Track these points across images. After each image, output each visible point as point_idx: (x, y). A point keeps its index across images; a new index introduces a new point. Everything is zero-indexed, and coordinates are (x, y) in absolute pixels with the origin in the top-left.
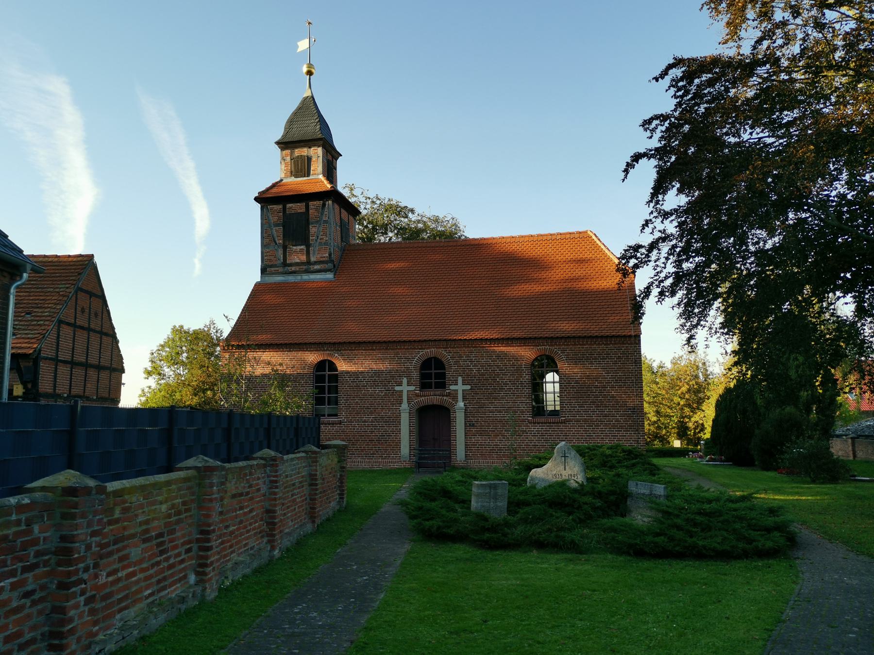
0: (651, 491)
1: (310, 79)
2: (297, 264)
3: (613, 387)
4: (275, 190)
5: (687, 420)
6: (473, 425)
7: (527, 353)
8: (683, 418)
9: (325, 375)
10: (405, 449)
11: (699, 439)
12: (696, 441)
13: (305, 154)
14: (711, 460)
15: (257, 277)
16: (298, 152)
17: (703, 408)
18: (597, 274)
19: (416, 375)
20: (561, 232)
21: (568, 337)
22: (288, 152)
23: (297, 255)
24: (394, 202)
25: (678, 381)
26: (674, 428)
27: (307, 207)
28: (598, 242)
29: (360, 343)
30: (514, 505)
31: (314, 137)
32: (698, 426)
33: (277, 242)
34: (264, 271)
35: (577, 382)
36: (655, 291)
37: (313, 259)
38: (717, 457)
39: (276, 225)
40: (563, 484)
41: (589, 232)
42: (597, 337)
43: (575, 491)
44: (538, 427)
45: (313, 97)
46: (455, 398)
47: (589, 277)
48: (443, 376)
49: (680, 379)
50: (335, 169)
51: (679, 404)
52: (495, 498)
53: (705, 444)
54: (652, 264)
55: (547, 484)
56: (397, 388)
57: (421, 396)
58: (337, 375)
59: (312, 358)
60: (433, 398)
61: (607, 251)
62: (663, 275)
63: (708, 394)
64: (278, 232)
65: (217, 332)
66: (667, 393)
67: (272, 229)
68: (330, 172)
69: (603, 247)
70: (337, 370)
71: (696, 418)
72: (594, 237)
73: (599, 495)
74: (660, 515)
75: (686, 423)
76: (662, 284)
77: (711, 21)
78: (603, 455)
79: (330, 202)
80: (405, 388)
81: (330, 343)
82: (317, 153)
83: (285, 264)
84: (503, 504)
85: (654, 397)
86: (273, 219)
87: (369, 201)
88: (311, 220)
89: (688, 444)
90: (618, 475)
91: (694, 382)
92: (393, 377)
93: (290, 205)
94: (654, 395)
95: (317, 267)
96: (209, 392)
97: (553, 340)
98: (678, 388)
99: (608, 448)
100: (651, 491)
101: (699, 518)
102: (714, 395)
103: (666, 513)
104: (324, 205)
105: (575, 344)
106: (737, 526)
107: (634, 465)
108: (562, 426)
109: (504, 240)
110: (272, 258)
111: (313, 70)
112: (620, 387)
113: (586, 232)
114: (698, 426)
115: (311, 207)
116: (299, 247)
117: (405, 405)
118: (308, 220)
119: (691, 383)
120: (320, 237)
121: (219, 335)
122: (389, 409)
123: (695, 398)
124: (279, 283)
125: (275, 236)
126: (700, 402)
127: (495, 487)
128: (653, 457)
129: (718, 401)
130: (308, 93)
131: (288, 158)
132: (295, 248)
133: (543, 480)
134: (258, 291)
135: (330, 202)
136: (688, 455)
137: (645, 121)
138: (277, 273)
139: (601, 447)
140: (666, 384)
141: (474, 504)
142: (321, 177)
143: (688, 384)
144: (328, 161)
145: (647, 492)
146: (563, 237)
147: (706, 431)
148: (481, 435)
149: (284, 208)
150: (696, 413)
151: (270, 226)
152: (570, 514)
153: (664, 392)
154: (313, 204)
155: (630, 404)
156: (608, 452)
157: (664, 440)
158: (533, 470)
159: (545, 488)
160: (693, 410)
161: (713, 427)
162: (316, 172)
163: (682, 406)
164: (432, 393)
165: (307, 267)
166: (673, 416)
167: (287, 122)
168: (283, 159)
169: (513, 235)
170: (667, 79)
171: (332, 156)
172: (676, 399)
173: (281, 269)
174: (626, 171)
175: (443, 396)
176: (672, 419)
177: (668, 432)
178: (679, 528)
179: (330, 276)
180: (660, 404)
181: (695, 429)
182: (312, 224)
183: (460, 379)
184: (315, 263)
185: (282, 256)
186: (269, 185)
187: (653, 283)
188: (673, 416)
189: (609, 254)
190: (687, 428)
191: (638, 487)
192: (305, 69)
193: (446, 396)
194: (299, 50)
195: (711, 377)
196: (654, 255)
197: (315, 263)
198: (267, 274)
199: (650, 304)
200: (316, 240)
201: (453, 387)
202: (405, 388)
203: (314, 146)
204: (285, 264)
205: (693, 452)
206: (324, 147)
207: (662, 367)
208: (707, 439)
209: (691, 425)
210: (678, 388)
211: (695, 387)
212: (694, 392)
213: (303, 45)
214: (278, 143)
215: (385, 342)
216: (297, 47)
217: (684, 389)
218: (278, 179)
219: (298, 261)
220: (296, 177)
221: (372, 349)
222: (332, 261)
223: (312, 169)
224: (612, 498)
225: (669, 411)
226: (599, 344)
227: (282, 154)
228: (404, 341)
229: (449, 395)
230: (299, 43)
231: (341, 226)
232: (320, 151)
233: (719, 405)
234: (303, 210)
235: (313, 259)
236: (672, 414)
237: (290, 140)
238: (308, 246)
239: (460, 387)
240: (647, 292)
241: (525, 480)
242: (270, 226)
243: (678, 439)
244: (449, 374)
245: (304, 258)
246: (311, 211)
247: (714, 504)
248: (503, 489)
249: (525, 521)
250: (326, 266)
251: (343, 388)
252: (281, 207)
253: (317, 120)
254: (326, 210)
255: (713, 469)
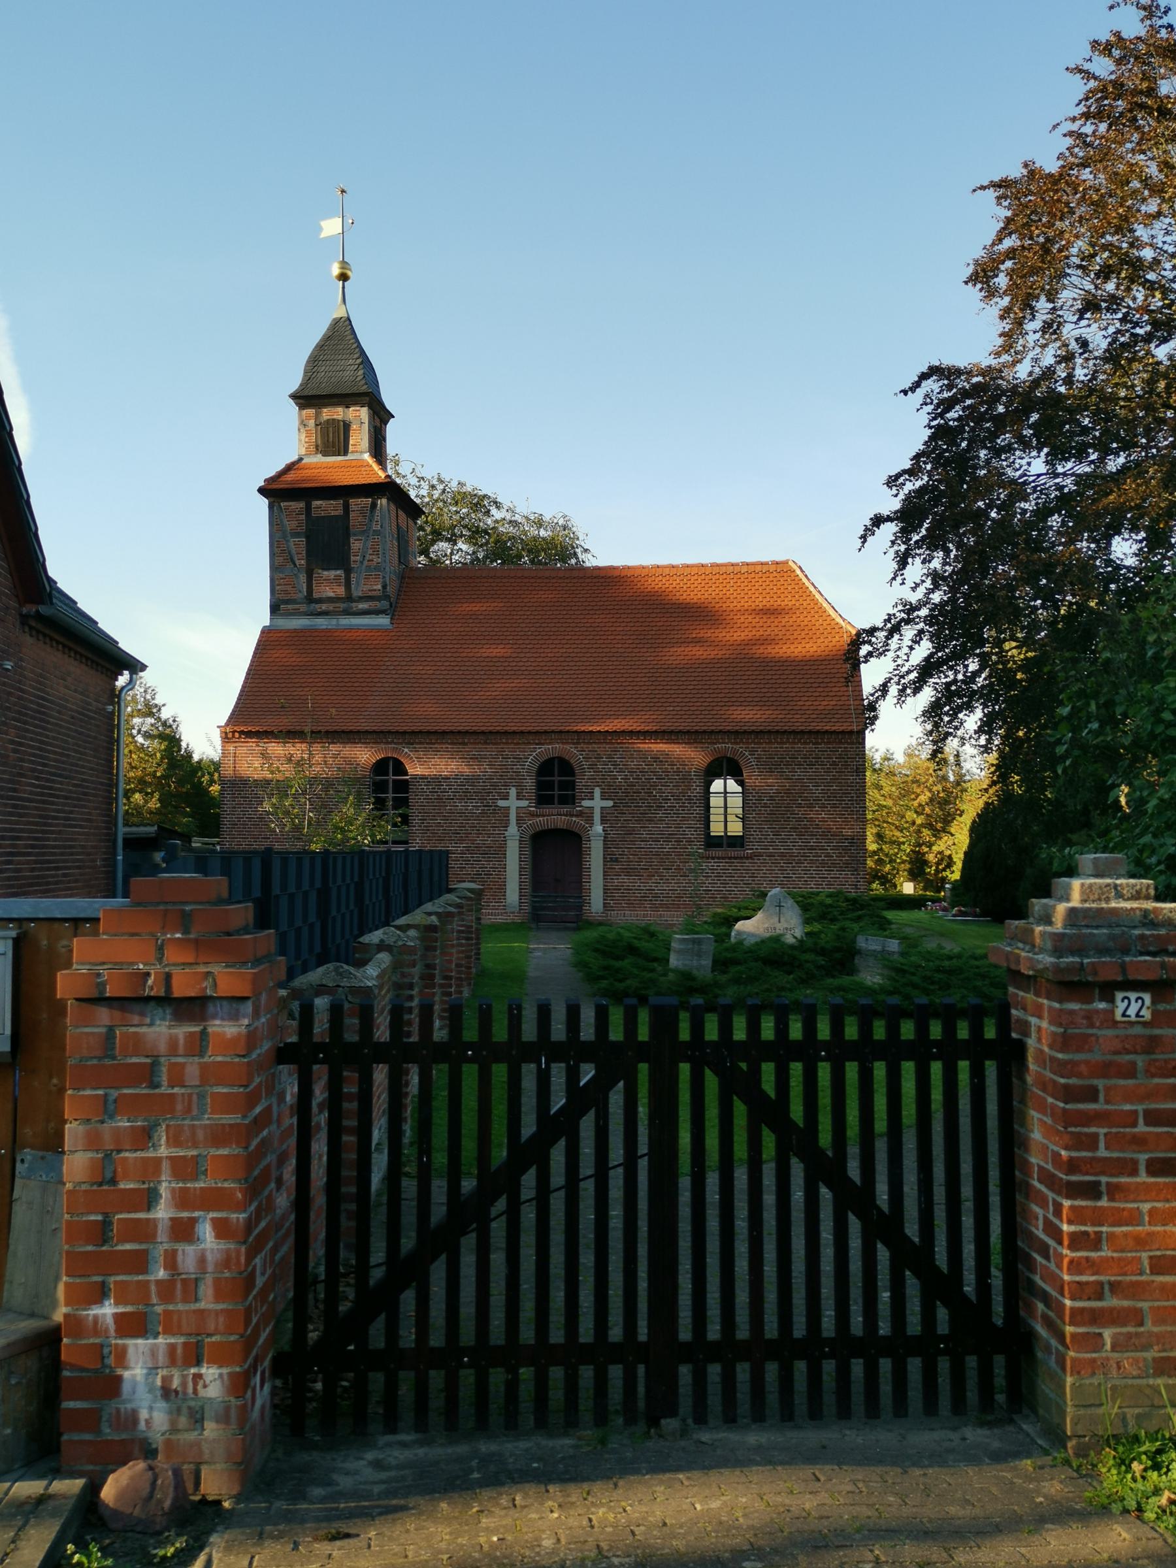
0: (884, 947)
1: (343, 288)
2: (330, 600)
3: (823, 806)
4: (290, 477)
5: (926, 849)
6: (616, 860)
7: (695, 756)
8: (920, 845)
9: (387, 781)
10: (512, 894)
11: (944, 880)
12: (938, 883)
13: (340, 417)
14: (961, 913)
15: (265, 619)
16: (327, 413)
17: (953, 830)
18: (803, 633)
19: (530, 783)
20: (749, 560)
21: (761, 732)
22: (311, 412)
23: (329, 584)
24: (469, 488)
25: (915, 785)
26: (903, 862)
27: (346, 507)
28: (804, 580)
29: (444, 733)
30: (721, 964)
31: (355, 390)
32: (942, 860)
33: (297, 562)
34: (275, 609)
35: (772, 799)
36: (893, 690)
37: (356, 593)
38: (968, 910)
39: (297, 535)
40: (777, 939)
41: (790, 563)
42: (802, 732)
43: (792, 947)
44: (712, 863)
45: (349, 319)
46: (590, 819)
47: (792, 637)
48: (571, 785)
49: (917, 781)
50: (385, 440)
51: (914, 823)
52: (699, 955)
53: (951, 890)
54: (891, 654)
55: (758, 940)
56: (501, 803)
57: (538, 816)
58: (407, 781)
59: (365, 756)
60: (556, 817)
61: (818, 596)
62: (904, 669)
63: (963, 807)
64: (297, 545)
65: (145, 691)
66: (895, 804)
67: (288, 541)
68: (378, 448)
69: (812, 588)
70: (406, 773)
71: (941, 846)
72: (798, 572)
73: (822, 952)
74: (893, 974)
75: (924, 854)
76: (903, 681)
77: (982, 305)
78: (822, 903)
79: (384, 501)
80: (513, 803)
81: (397, 732)
82: (359, 416)
83: (310, 599)
84: (707, 962)
85: (874, 811)
86: (290, 525)
87: (425, 485)
88: (352, 530)
89: (925, 889)
90: (843, 929)
91: (939, 787)
92: (495, 786)
93: (319, 503)
94: (875, 808)
95: (363, 606)
96: (137, 796)
97: (738, 735)
98: (913, 796)
99: (827, 896)
100: (884, 947)
101: (938, 976)
102: (971, 808)
103: (900, 971)
104: (374, 505)
105: (770, 743)
106: (979, 983)
107: (859, 918)
108: (747, 863)
109: (660, 571)
110: (289, 588)
111: (349, 273)
112: (834, 806)
113: (786, 562)
114: (942, 860)
115: (353, 507)
116: (332, 574)
117: (513, 829)
118: (348, 528)
119: (935, 789)
120: (368, 557)
121: (148, 697)
122: (489, 835)
123: (940, 813)
124: (301, 631)
125: (294, 552)
126: (948, 819)
127: (699, 942)
128: (888, 909)
129: (974, 822)
130: (340, 313)
131: (312, 423)
132: (326, 573)
133: (753, 935)
134: (268, 642)
135: (384, 501)
136: (925, 906)
137: (890, 477)
138: (297, 613)
139: (818, 894)
140: (894, 789)
141: (674, 961)
142: (367, 456)
143: (930, 791)
144: (375, 427)
145: (879, 948)
146: (751, 569)
147: (954, 868)
148: (628, 874)
149: (308, 508)
150: (940, 838)
151: (284, 537)
152: (789, 973)
153: (889, 803)
154: (357, 503)
155: (848, 832)
156: (829, 901)
157: (885, 880)
158: (740, 923)
159: (757, 944)
160: (937, 834)
161: (965, 862)
162: (359, 448)
163: (919, 826)
164: (555, 811)
165: (347, 604)
166: (904, 843)
167: (308, 362)
168: (303, 424)
169: (675, 563)
170: (920, 392)
171: (381, 416)
172: (910, 815)
173: (303, 608)
174: (864, 538)
175: (572, 816)
176: (902, 847)
177: (894, 868)
178: (915, 986)
179: (383, 621)
180: (884, 822)
181: (938, 864)
182: (355, 535)
183: (597, 792)
184: (361, 599)
185: (305, 585)
186: (280, 466)
187: (891, 679)
188: (904, 843)
189: (821, 600)
190: (926, 863)
191: (868, 943)
192: (336, 270)
193: (577, 816)
194: (323, 235)
195: (967, 778)
196: (894, 642)
197: (361, 599)
198: (282, 615)
199: (886, 707)
200: (362, 563)
201: (586, 803)
202: (513, 803)
203: (355, 404)
204: (310, 599)
205: (933, 901)
206: (370, 407)
207: (889, 759)
208: (956, 881)
209: (931, 858)
210: (913, 796)
211: (941, 795)
212: (939, 803)
213: (331, 227)
214: (295, 397)
215: (483, 733)
216: (321, 229)
217: (924, 798)
218: (295, 458)
219: (332, 595)
220: (325, 454)
221: (463, 743)
222: (387, 597)
223: (351, 442)
224: (838, 955)
225: (898, 834)
226: (805, 743)
227: (300, 415)
228: (514, 733)
229: (580, 814)
230: (324, 224)
231: (398, 539)
232: (364, 413)
233: (974, 829)
234: (340, 512)
235: (356, 593)
236: (902, 840)
237: (314, 392)
238: (348, 571)
239: (597, 803)
240: (884, 689)
241: (729, 935)
242: (284, 537)
243: (910, 880)
244: (581, 782)
245: (341, 591)
246: (352, 515)
247: (955, 961)
248: (709, 947)
249: (737, 981)
250: (378, 605)
251: (417, 800)
252: (302, 505)
253: (359, 361)
254: (377, 513)
255: (962, 927)
